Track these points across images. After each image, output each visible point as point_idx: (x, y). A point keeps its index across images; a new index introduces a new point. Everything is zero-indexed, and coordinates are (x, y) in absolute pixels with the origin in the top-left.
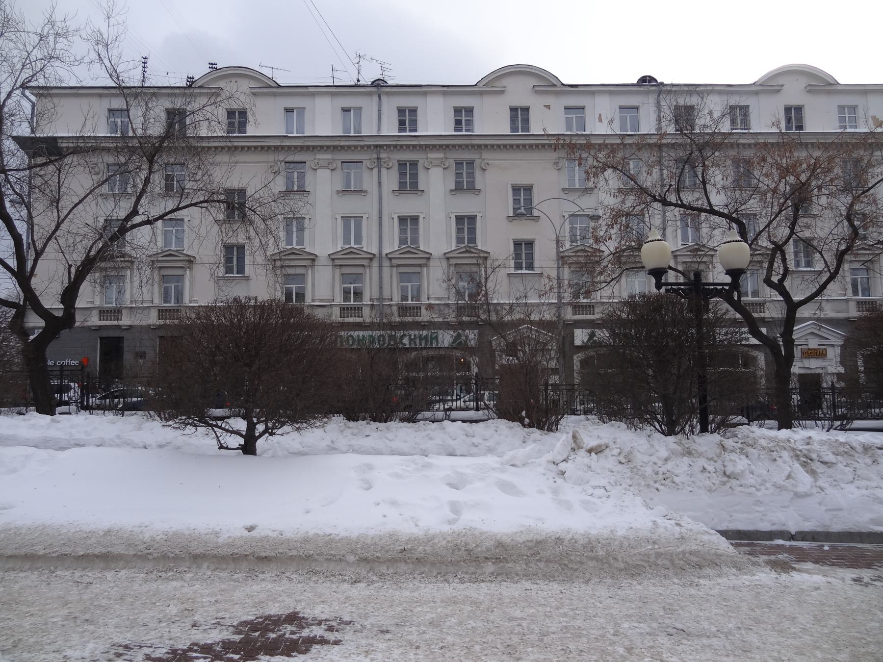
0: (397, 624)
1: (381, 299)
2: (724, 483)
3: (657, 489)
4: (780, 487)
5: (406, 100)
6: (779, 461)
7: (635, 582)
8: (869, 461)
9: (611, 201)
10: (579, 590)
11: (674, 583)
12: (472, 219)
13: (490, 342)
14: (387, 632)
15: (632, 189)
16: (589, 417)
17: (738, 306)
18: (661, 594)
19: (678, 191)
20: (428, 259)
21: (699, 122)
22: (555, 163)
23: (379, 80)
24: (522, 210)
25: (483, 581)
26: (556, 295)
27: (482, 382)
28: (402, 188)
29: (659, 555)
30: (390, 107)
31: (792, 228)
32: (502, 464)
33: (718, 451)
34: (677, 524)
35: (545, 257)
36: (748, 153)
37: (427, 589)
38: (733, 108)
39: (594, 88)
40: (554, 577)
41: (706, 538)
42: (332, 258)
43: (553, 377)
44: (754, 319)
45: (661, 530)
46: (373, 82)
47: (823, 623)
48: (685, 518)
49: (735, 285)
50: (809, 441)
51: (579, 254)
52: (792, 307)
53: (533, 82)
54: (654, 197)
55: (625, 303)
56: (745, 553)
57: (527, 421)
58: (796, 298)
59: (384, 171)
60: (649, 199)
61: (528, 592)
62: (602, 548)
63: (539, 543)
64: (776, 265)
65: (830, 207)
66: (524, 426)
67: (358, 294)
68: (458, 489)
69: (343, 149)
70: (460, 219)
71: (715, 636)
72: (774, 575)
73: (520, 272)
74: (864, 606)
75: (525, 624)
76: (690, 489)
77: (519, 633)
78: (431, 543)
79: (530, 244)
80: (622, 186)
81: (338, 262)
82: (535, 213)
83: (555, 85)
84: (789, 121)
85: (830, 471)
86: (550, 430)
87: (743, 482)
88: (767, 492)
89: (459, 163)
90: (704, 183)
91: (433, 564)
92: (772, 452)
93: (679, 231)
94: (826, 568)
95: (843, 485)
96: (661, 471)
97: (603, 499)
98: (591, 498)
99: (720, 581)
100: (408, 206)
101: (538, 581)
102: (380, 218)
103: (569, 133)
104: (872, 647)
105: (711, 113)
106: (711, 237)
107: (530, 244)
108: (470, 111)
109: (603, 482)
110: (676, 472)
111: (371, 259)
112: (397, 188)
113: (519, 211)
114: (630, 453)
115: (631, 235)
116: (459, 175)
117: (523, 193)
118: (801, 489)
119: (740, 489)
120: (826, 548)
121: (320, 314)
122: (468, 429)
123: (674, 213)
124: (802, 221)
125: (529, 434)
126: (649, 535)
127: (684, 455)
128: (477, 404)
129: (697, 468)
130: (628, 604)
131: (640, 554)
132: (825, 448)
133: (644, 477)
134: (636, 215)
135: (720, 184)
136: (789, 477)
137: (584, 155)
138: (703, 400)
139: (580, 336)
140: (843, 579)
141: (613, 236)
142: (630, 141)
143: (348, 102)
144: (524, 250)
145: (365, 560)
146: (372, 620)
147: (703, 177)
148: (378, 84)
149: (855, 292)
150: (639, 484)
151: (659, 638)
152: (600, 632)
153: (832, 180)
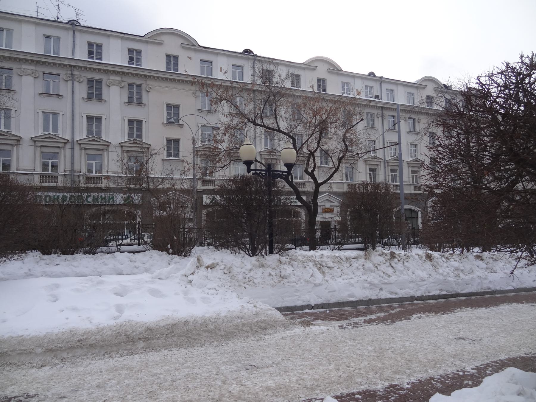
0: (72, 391)
1: (72, 171)
2: (280, 282)
3: (245, 287)
4: (307, 282)
5: (97, 39)
6: (308, 268)
7: (230, 342)
8: (348, 265)
9: (225, 120)
10: (198, 351)
11: (252, 340)
12: (139, 122)
13: (150, 202)
14: (64, 397)
15: (237, 114)
16: (210, 247)
17: (290, 184)
18: (244, 347)
19: (262, 117)
20: (108, 146)
21: (275, 80)
22: (193, 93)
23: (74, 20)
24: (172, 120)
25: (137, 354)
26: (192, 173)
27: (145, 227)
28: (90, 96)
29: (244, 325)
30: (82, 41)
31: (318, 143)
32: (153, 278)
33: (278, 264)
34: (254, 306)
35: (186, 150)
36: (298, 101)
37: (96, 364)
38: (292, 75)
39: (398, 82)
40: (182, 345)
41: (269, 312)
42: (34, 140)
43: (188, 223)
44: (299, 191)
45: (246, 310)
46: (69, 21)
47: (324, 351)
48: (259, 302)
49: (289, 172)
50: (322, 256)
51: (205, 149)
52: (318, 186)
53: (181, 41)
54: (249, 119)
55: (230, 180)
56: (289, 319)
57: (171, 250)
58: (319, 181)
59: (76, 83)
60: (246, 120)
61: (166, 357)
62: (212, 324)
63: (173, 325)
64: (310, 163)
65: (335, 134)
66: (169, 254)
67: (55, 167)
68: (122, 296)
69: (46, 65)
70: (131, 122)
71: (271, 366)
72: (302, 329)
73: (171, 158)
74: (343, 339)
75: (162, 376)
76: (263, 286)
77: (158, 383)
78: (101, 333)
79: (177, 141)
80: (231, 111)
81: (38, 144)
82: (181, 122)
83: (195, 46)
84: (319, 86)
85: (331, 271)
86: (185, 256)
87: (290, 280)
88: (301, 285)
89: (131, 85)
90: (275, 114)
91: (102, 347)
92: (304, 263)
93: (263, 140)
94: (327, 322)
95: (337, 278)
96: (247, 277)
97: (214, 296)
98: (207, 296)
99: (275, 335)
100: (94, 109)
101: (172, 349)
102: (73, 115)
103: (203, 76)
104: (345, 360)
105: (280, 76)
106: (279, 145)
107: (177, 141)
108: (139, 52)
109: (215, 285)
110: (255, 277)
111: (65, 143)
112: (86, 97)
113: (170, 120)
114: (231, 267)
115: (236, 141)
116: (131, 93)
117: (173, 110)
118: (317, 282)
119: (288, 284)
120: (328, 312)
121: (22, 180)
122: (132, 257)
123: (259, 129)
124: (323, 140)
125: (172, 259)
126: (239, 314)
127: (260, 267)
128: (139, 241)
129: (266, 274)
130: (225, 355)
131: (233, 325)
132: (329, 259)
133: (238, 281)
134: (239, 129)
135: (284, 116)
136: (312, 276)
137: (210, 90)
138: (271, 236)
139: (206, 199)
140: (334, 327)
141: (226, 141)
142: (236, 86)
143: (49, 32)
144: (173, 144)
145: (51, 350)
146: (53, 391)
147: (275, 111)
148: (73, 24)
149: (347, 179)
150: (235, 285)
151: (241, 372)
152: (208, 374)
153: (336, 120)
